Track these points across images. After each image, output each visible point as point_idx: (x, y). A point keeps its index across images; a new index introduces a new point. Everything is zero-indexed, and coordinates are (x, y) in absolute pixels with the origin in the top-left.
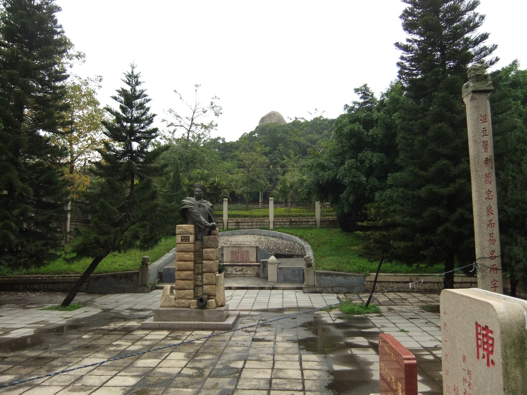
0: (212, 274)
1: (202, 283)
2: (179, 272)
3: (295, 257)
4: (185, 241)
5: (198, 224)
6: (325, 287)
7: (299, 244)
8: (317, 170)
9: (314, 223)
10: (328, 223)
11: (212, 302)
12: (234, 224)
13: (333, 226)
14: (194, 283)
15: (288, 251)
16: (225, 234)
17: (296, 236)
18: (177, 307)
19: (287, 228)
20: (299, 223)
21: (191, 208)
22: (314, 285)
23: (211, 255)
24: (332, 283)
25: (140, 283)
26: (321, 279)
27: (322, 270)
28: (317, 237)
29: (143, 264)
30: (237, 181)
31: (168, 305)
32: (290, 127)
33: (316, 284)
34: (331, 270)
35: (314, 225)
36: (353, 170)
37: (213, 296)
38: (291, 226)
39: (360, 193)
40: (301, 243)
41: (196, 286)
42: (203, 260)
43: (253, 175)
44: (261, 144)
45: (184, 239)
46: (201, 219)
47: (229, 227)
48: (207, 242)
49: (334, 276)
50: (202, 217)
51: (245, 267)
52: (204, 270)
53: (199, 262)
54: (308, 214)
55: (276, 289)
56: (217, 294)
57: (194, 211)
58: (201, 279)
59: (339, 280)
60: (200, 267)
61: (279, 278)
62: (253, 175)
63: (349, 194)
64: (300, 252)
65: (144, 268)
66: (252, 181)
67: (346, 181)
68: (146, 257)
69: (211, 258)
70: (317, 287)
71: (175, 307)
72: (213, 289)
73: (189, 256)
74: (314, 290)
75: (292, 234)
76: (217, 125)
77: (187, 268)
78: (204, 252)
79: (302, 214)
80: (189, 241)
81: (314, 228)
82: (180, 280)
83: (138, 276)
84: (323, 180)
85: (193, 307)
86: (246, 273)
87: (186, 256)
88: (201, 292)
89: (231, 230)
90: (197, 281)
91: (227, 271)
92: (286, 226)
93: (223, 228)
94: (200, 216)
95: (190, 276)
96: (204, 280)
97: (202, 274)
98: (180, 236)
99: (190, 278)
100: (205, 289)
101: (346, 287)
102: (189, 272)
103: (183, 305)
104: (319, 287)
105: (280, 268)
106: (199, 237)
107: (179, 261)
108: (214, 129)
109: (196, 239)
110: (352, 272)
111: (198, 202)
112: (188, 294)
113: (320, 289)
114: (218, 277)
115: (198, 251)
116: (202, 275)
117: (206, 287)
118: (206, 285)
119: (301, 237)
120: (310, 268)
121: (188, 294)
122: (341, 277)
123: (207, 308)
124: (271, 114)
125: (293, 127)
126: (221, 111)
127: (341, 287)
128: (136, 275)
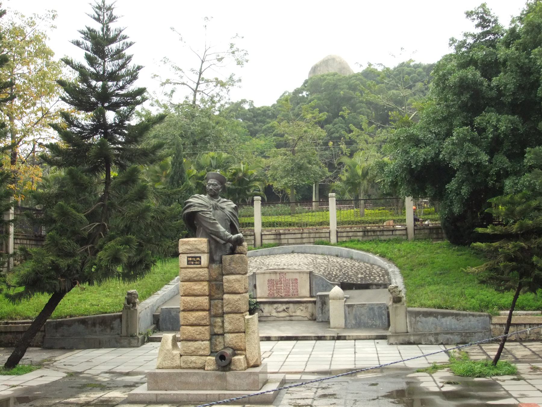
0: (238, 316)
1: (223, 331)
3: (374, 287)
4: (194, 264)
5: (214, 236)
6: (424, 335)
7: (379, 266)
9: (404, 232)
11: (239, 359)
12: (272, 237)
13: (435, 236)
16: (258, 253)
17: (375, 253)
18: (184, 368)
19: (359, 241)
20: (378, 233)
21: (202, 211)
24: (436, 329)
25: (124, 332)
26: (418, 321)
27: (419, 307)
28: (409, 255)
29: (129, 303)
32: (360, 79)
34: (435, 307)
35: (404, 235)
36: (466, 144)
37: (242, 350)
38: (365, 239)
40: (382, 266)
45: (192, 261)
46: (217, 228)
47: (265, 242)
48: (230, 265)
49: (439, 317)
50: (219, 226)
51: (291, 305)
52: (226, 309)
53: (217, 296)
55: (344, 338)
56: (247, 347)
57: (208, 216)
58: (221, 324)
60: (220, 306)
61: (348, 321)
62: (301, 159)
65: (129, 308)
66: (300, 168)
67: (455, 162)
70: (410, 335)
71: (181, 368)
72: (241, 339)
73: (200, 287)
74: (407, 339)
75: (368, 251)
76: (240, 80)
80: (200, 264)
82: (186, 325)
83: (121, 321)
85: (209, 368)
86: (294, 314)
87: (196, 287)
88: (222, 344)
90: (215, 326)
91: (262, 312)
92: (358, 238)
93: (255, 245)
94: (217, 223)
95: (203, 319)
96: (226, 325)
97: (222, 315)
98: (186, 256)
99: (203, 322)
100: (228, 340)
101: (460, 334)
102: (201, 313)
103: (194, 365)
104: (414, 335)
105: (349, 306)
106: (217, 258)
107: (185, 296)
109: (212, 260)
112: (200, 348)
113: (417, 338)
114: (248, 320)
116: (223, 317)
117: (228, 337)
118: (228, 333)
119: (383, 256)
120: (398, 305)
121: (200, 348)
122: (450, 318)
123: (232, 370)
127: (452, 334)
128: (118, 320)
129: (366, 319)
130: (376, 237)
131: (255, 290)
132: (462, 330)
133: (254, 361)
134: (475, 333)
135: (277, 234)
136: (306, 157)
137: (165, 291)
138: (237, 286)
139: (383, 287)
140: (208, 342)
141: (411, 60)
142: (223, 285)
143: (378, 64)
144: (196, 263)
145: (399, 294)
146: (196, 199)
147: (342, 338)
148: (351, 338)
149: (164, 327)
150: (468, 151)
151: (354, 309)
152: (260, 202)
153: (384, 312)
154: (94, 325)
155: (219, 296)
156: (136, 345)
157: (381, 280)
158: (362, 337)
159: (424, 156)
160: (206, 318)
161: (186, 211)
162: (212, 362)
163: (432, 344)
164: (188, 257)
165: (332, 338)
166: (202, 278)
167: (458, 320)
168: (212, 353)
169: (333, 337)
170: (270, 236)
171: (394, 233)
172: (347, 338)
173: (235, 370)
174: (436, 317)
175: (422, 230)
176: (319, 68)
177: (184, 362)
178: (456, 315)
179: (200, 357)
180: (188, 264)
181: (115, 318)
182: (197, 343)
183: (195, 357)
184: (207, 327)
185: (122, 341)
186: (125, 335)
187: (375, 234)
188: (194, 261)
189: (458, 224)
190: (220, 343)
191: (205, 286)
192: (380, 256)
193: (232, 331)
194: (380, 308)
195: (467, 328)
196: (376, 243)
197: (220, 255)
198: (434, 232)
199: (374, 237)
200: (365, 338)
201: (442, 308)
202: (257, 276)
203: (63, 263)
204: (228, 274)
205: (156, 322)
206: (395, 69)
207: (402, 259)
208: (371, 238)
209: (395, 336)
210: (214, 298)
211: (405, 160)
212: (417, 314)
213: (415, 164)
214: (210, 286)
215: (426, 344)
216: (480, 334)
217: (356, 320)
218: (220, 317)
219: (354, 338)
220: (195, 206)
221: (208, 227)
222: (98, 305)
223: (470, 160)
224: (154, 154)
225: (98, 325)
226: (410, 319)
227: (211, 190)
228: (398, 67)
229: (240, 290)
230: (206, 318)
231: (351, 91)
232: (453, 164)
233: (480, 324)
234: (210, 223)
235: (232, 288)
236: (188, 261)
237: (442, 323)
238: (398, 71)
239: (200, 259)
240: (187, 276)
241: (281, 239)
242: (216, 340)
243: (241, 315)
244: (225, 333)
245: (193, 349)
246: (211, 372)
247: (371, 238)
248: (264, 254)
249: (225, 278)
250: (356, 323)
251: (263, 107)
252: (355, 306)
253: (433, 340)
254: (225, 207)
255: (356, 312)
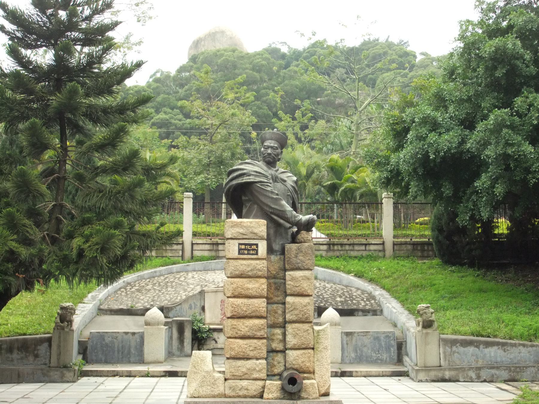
0: (306, 326)
1: (285, 346)
2: (234, 322)
3: (360, 313)
4: (248, 254)
5: (275, 217)
6: (462, 369)
7: (358, 289)
8: (424, 131)
9: (380, 247)
10: (410, 247)
11: (312, 384)
12: (207, 247)
13: (420, 254)
14: (267, 346)
15: (341, 302)
16: (190, 268)
17: (349, 272)
18: (230, 397)
19: (322, 256)
20: (347, 247)
21: (261, 182)
22: (439, 365)
23: (305, 286)
24: (477, 362)
25: (54, 362)
26: (454, 352)
27: (452, 334)
28: (395, 276)
29: (62, 321)
30: (188, 162)
31: (209, 392)
32: (266, 59)
33: (443, 363)
34: (473, 335)
35: (380, 251)
36: (505, 131)
37: (309, 372)
38: (330, 254)
39: (518, 178)
40: (363, 288)
41: (271, 351)
42: (286, 295)
43: (224, 151)
44: (242, 84)
45: (245, 249)
46: (282, 206)
47: (197, 253)
48: (296, 257)
49: (481, 346)
50: (284, 202)
52: (288, 317)
53: (276, 299)
54: (345, 233)
55: (350, 374)
56: (317, 369)
57: (269, 189)
58: (280, 337)
59: (492, 354)
60: (280, 312)
61: (346, 354)
62: (224, 151)
63: (494, 181)
64: (367, 305)
65: (63, 328)
66: (221, 162)
67: (490, 152)
68: (68, 304)
69: (305, 290)
70: (445, 370)
71: (225, 396)
72: (309, 357)
73: (257, 285)
74: (440, 375)
75: (337, 269)
76: (140, 43)
77: (254, 311)
78: (288, 278)
79: (331, 232)
80: (257, 254)
81: (380, 257)
82: (236, 338)
83: (50, 346)
84: (437, 152)
85: (271, 396)
87: (250, 286)
88: (282, 364)
89: (201, 259)
90: (273, 340)
91: (216, 342)
92: (321, 252)
93: (182, 256)
94: (280, 199)
95: (260, 329)
96: (289, 338)
97: (283, 326)
98: (236, 242)
99: (259, 334)
100: (292, 359)
101: (508, 368)
102: (257, 322)
103: (245, 392)
104: (450, 369)
105: (348, 334)
106: (277, 247)
107: (235, 297)
108: (133, 51)
109: (270, 250)
110: (516, 337)
111: (272, 172)
112: (255, 369)
113: (453, 373)
114: (318, 332)
115: (275, 277)
116: (284, 327)
117: (292, 355)
118: (291, 349)
119: (359, 275)
120: (429, 331)
121: (255, 369)
122: (495, 348)
123: (303, 399)
124: (216, 32)
125: (272, 60)
126: (151, 13)
127: (498, 368)
128: (46, 345)
129: (369, 351)
130: (345, 252)
131: (203, 314)
132: (509, 364)
133: (326, 388)
134: (526, 367)
135: (213, 244)
136: (229, 149)
137: (83, 311)
138: (305, 285)
139: (371, 313)
140: (264, 362)
141: (325, 40)
142: (285, 283)
143: (282, 43)
144: (251, 252)
145: (431, 317)
146: (250, 166)
147: (347, 374)
148: (359, 374)
149: (94, 358)
150: (508, 140)
151: (354, 339)
152: (191, 201)
153: (392, 342)
154: (10, 350)
155: (279, 299)
156: (71, 379)
157: (367, 305)
158: (374, 374)
159: (448, 144)
160: (264, 329)
161: (234, 182)
162: (275, 388)
163: (472, 382)
164: (240, 244)
165: (334, 374)
166: (260, 273)
167: (505, 351)
168: (270, 376)
169: (336, 372)
170: (204, 246)
171: (367, 248)
172: (354, 374)
173: (307, 398)
174: (477, 347)
175: (404, 246)
176: (203, 43)
177: (230, 388)
178: (504, 345)
179: (253, 382)
180: (239, 253)
181: (41, 341)
182: (250, 362)
183: (246, 381)
184: (265, 341)
185: (52, 374)
186: (56, 365)
187: (343, 248)
188: (249, 250)
189: (455, 239)
190: (279, 363)
191: (263, 284)
192: (356, 275)
193: (296, 347)
194: (387, 337)
195: (515, 361)
196: (344, 259)
197: (281, 243)
198: (419, 248)
199: (342, 252)
200: (377, 374)
201: (482, 336)
202: (206, 294)
203: (24, 252)
204: (293, 269)
205: (82, 351)
206: (304, 50)
207: (387, 280)
208: (338, 253)
209: (425, 370)
210: (272, 301)
211: (420, 148)
212: (454, 342)
213: (435, 154)
214: (269, 285)
215: (464, 381)
216: (533, 369)
217: (357, 352)
218: (280, 327)
219: (363, 374)
220: (249, 175)
221: (269, 204)
222: (7, 325)
223: (510, 151)
224: (134, 112)
225: (16, 351)
226: (445, 349)
227: (269, 154)
228: (308, 48)
229: (309, 291)
230: (264, 329)
231: (254, 73)
232: (487, 156)
233: (532, 357)
234: (273, 198)
235: (299, 288)
236: (240, 250)
237: (485, 354)
238: (308, 52)
239: (257, 247)
240: (238, 270)
241: (218, 250)
242: (273, 359)
243: (310, 325)
244: (286, 349)
245: (244, 370)
246: (273, 401)
247: (338, 253)
248: (197, 269)
249: (289, 274)
250: (356, 356)
251: (136, 87)
252: (356, 335)
253: (474, 376)
254: (286, 179)
255: (356, 342)
